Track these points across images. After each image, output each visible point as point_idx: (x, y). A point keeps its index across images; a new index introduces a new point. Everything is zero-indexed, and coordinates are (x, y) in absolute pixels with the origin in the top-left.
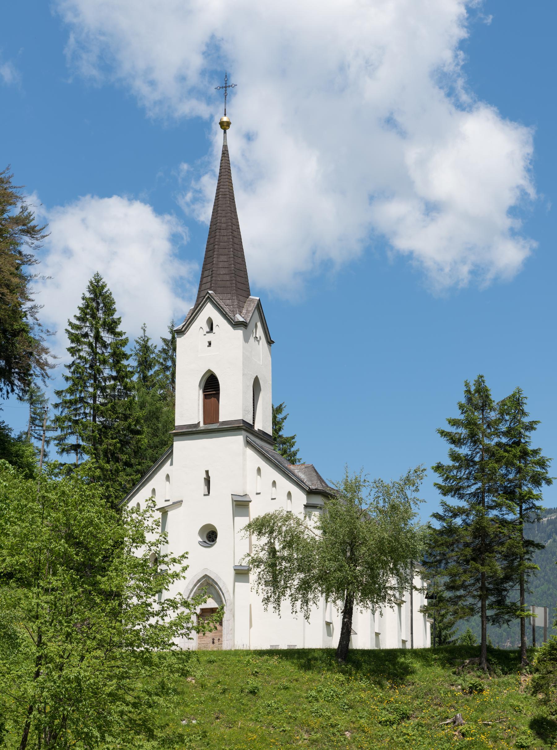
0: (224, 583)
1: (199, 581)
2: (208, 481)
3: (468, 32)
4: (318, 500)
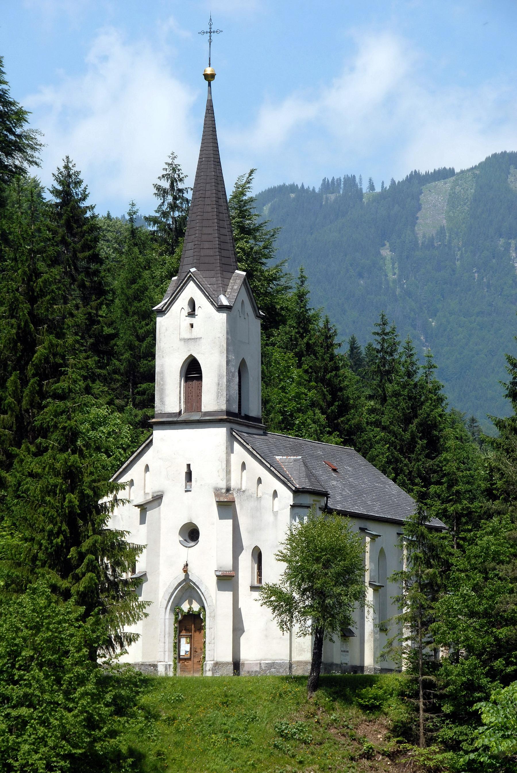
0: (206, 588)
1: (179, 584)
2: (189, 476)
3: (319, 191)
4: (308, 500)
